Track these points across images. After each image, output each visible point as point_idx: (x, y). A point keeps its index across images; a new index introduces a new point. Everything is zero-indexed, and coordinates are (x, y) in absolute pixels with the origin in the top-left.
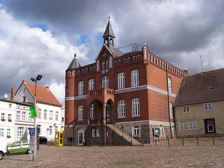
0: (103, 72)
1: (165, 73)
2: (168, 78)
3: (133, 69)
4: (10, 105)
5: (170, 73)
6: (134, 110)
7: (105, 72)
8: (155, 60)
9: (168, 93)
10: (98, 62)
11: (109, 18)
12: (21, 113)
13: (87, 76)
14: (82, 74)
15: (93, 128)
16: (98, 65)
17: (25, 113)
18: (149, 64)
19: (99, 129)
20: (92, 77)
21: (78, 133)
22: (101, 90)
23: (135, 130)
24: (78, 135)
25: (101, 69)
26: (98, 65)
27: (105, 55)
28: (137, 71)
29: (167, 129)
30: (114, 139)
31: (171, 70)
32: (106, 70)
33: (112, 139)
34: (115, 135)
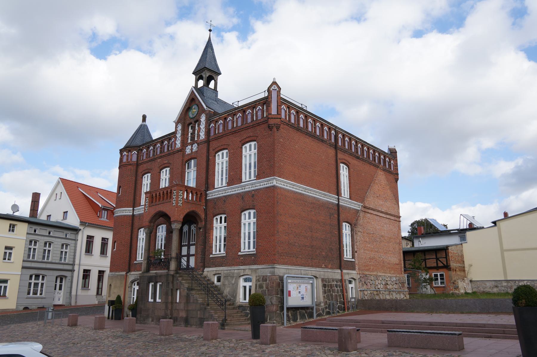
0: (188, 151)
1: (332, 152)
2: (342, 165)
3: (247, 140)
4: (14, 226)
5: (345, 151)
6: (347, 250)
7: (192, 149)
8: (382, 160)
9: (338, 199)
10: (180, 127)
11: (207, 22)
12: (39, 247)
13: (159, 160)
14: (149, 157)
15: (150, 280)
16: (179, 135)
17: (67, 245)
18: (282, 126)
19: (161, 283)
20: (167, 162)
21: (134, 289)
22: (171, 190)
23: (245, 287)
24: (134, 295)
25: (184, 144)
26: (179, 135)
27: (194, 110)
28: (255, 145)
29: (331, 286)
30: (190, 308)
31: (363, 152)
32: (194, 145)
33: (186, 309)
34: (191, 301)
